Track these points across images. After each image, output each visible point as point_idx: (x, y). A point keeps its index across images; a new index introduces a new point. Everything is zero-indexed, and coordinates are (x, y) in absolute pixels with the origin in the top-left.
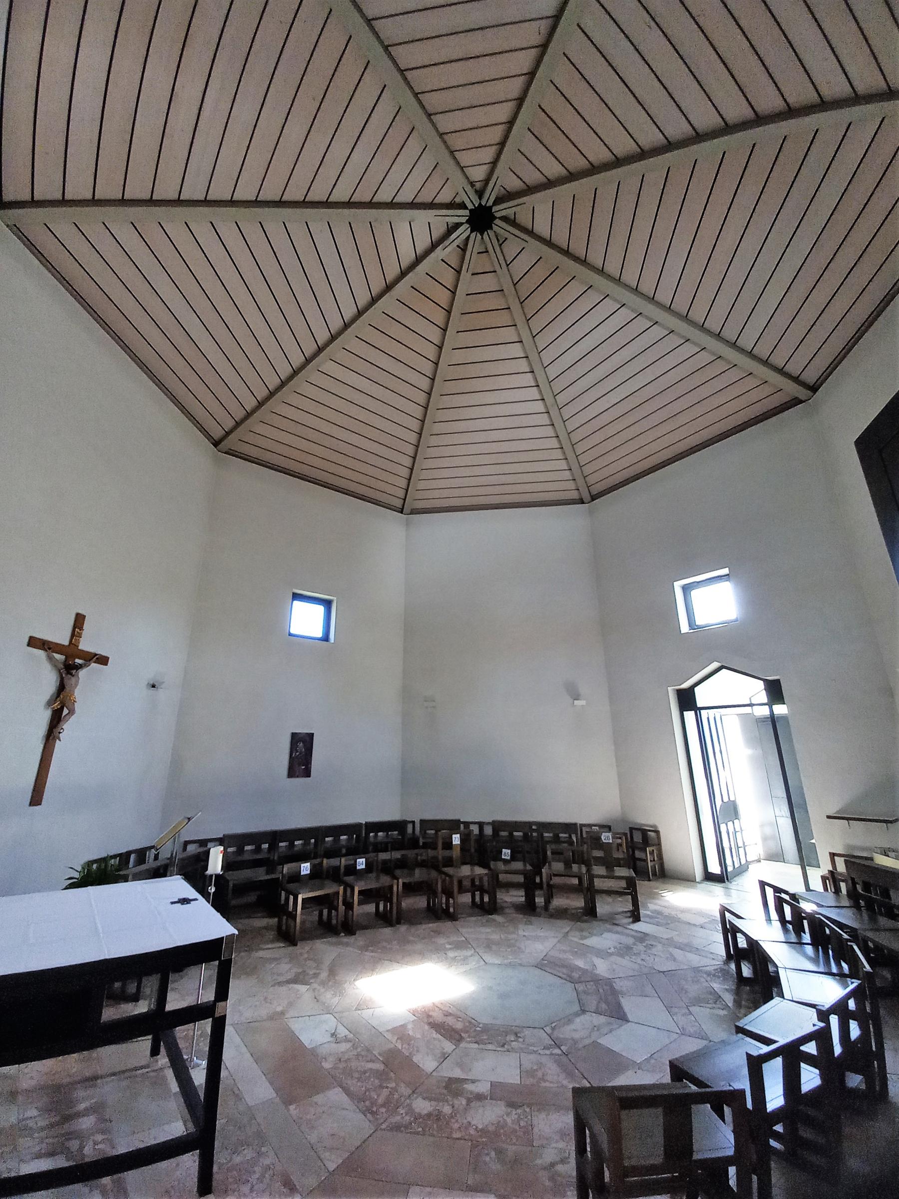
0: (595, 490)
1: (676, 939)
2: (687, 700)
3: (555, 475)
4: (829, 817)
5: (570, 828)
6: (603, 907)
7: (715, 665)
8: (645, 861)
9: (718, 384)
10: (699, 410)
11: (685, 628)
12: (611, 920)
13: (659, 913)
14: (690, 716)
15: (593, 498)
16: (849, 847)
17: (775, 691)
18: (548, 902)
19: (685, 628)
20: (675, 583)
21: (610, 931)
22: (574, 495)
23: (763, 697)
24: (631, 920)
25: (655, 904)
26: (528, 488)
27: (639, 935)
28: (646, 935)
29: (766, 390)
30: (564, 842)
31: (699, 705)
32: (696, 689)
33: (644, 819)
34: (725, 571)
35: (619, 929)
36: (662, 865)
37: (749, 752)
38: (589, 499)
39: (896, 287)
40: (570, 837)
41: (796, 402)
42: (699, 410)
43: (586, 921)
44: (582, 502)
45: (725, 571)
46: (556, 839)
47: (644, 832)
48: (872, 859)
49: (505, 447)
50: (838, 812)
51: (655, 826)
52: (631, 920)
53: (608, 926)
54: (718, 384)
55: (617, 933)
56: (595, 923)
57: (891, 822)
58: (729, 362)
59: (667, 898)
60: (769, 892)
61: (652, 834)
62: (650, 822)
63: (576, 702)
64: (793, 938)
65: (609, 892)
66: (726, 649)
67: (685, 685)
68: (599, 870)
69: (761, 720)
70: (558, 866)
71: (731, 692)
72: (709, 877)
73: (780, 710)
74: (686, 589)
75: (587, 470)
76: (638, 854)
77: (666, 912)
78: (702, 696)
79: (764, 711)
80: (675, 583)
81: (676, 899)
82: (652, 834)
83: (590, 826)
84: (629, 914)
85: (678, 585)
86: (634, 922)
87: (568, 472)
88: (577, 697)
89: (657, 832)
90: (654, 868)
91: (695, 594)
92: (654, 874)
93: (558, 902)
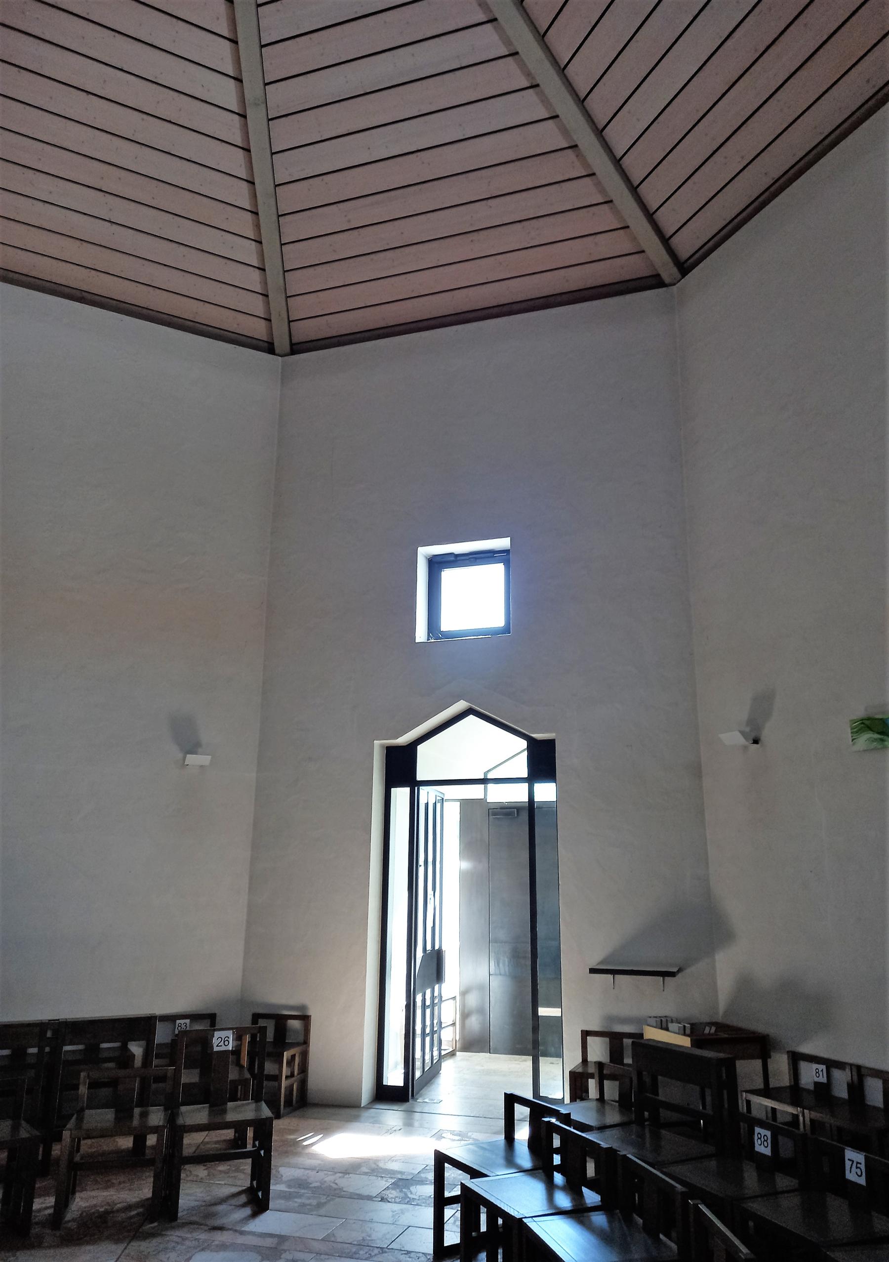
0: (306, 331)
1: (342, 1235)
2: (401, 767)
3: (225, 274)
4: (593, 971)
5: (141, 1027)
6: (191, 1194)
7: (461, 705)
8: (277, 1078)
9: (555, 199)
10: (513, 238)
11: (421, 634)
12: (207, 1220)
13: (301, 1184)
14: (401, 795)
15: (296, 348)
16: (610, 1019)
17: (542, 761)
18: (62, 1205)
19: (421, 634)
20: (420, 549)
21: (204, 1247)
22: (258, 329)
23: (521, 767)
24: (248, 1211)
25: (296, 1166)
26: (161, 277)
27: (269, 1242)
28: (282, 1239)
29: (619, 243)
30: (109, 1060)
31: (419, 778)
32: (420, 748)
33: (280, 996)
34: (503, 543)
35: (220, 1237)
36: (303, 1083)
37: (466, 865)
38: (287, 348)
39: (885, 90)
40: (124, 1048)
41: (655, 282)
42: (513, 238)
43: (152, 1235)
44: (270, 348)
45: (503, 543)
46: (92, 1056)
47: (280, 1020)
48: (641, 1035)
49: (127, 155)
50: (601, 963)
51: (303, 1008)
52: (248, 1211)
53: (203, 1236)
54: (555, 199)
55: (223, 1247)
56: (174, 1235)
57: (672, 974)
58: (585, 163)
59: (316, 1149)
60: (521, 1111)
61: (295, 1024)
62: (292, 1002)
63: (191, 759)
64: (563, 1201)
65: (202, 1158)
66: (485, 683)
67: (404, 740)
68: (194, 1114)
69: (507, 811)
70: (103, 1117)
71: (475, 757)
72: (385, 1095)
73: (546, 792)
74: (436, 564)
75: (298, 283)
76: (270, 1067)
77: (315, 1178)
78: (430, 761)
79: (518, 794)
80: (420, 549)
81: (335, 1146)
82: (295, 1024)
83: (171, 1019)
84: (243, 1199)
85: (425, 552)
86: (255, 1214)
87: (256, 275)
88: (193, 748)
89: (305, 1019)
90: (290, 1089)
91: (448, 576)
92: (289, 1102)
93: (86, 1200)
